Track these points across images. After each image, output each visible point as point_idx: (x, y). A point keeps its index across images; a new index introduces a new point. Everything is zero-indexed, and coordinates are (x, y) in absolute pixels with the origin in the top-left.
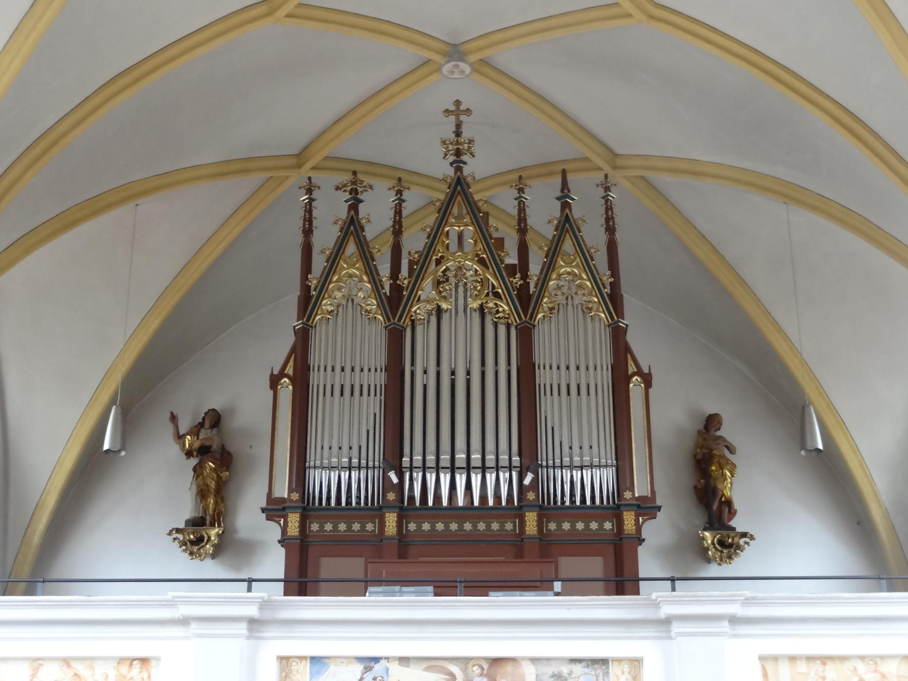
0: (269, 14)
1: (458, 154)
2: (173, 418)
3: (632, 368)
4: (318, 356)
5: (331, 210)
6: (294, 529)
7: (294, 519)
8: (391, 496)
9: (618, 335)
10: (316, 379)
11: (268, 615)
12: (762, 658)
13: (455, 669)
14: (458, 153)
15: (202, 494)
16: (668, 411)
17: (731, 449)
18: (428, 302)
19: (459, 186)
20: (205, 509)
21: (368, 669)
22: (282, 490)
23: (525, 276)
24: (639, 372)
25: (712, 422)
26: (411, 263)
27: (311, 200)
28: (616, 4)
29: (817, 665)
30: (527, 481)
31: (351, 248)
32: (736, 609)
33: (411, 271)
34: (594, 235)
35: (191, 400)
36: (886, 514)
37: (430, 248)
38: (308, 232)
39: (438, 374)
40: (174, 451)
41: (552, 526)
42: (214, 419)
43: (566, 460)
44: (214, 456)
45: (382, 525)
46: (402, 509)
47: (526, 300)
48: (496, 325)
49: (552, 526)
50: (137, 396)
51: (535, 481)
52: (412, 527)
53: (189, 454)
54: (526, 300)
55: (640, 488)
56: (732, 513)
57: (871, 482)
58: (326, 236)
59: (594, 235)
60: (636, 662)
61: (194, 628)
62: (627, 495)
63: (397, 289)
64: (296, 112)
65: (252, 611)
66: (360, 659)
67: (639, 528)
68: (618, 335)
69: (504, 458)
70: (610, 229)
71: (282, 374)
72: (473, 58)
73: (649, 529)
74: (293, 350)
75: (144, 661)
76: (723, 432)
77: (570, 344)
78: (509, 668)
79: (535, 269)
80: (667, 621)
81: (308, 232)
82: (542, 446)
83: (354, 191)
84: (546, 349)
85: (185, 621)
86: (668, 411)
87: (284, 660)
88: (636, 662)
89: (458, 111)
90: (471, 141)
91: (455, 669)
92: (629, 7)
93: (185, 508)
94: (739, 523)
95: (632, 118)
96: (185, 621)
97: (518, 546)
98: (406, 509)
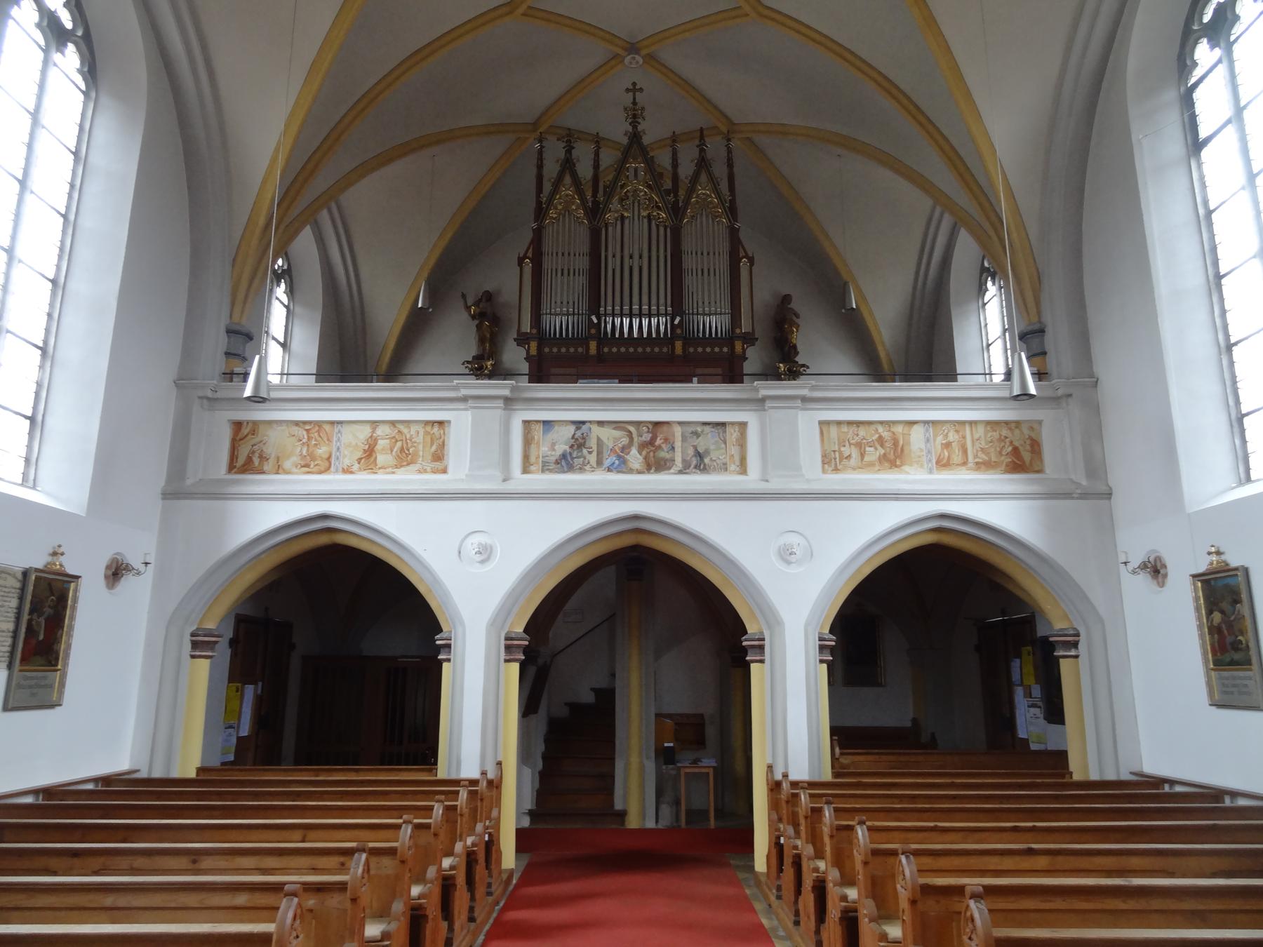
0: (511, 13)
1: (635, 114)
2: (464, 296)
3: (742, 253)
4: (547, 246)
5: (554, 152)
6: (534, 351)
7: (534, 345)
8: (593, 331)
9: (734, 234)
10: (547, 263)
11: (516, 395)
12: (821, 423)
13: (632, 429)
14: (635, 116)
15: (482, 340)
16: (765, 284)
17: (797, 316)
18: (616, 211)
19: (635, 137)
20: (484, 349)
21: (578, 429)
22: (526, 328)
23: (676, 195)
24: (746, 256)
25: (786, 299)
26: (605, 187)
27: (542, 147)
28: (740, 7)
29: (854, 428)
30: (676, 322)
31: (568, 180)
32: (805, 392)
33: (605, 192)
34: (720, 170)
35: (476, 283)
36: (888, 355)
37: (616, 179)
38: (540, 167)
39: (622, 257)
40: (464, 316)
41: (691, 350)
42: (488, 297)
43: (700, 310)
44: (489, 319)
45: (588, 349)
46: (599, 338)
47: (677, 211)
48: (658, 226)
49: (691, 350)
50: (442, 280)
51: (681, 321)
52: (606, 350)
53: (473, 317)
54: (677, 211)
55: (745, 327)
56: (797, 353)
57: (879, 333)
58: (551, 169)
59: (720, 170)
60: (743, 425)
61: (471, 403)
62: (738, 331)
63: (596, 203)
64: (529, 93)
65: (507, 392)
66: (574, 422)
67: (744, 351)
68: (734, 234)
69: (662, 308)
70: (730, 165)
71: (525, 257)
72: (644, 52)
73: (751, 352)
74: (532, 242)
75: (441, 423)
76: (792, 305)
77: (704, 239)
78: (665, 428)
79: (682, 193)
80: (763, 400)
81: (540, 167)
82: (686, 300)
83: (569, 141)
84: (688, 244)
85: (465, 399)
86: (765, 284)
87: (526, 423)
88: (743, 425)
89: (634, 89)
90: (643, 109)
91: (632, 429)
92: (747, 9)
93: (472, 350)
94: (800, 359)
95: (744, 95)
96: (465, 399)
97: (671, 359)
98: (603, 339)
